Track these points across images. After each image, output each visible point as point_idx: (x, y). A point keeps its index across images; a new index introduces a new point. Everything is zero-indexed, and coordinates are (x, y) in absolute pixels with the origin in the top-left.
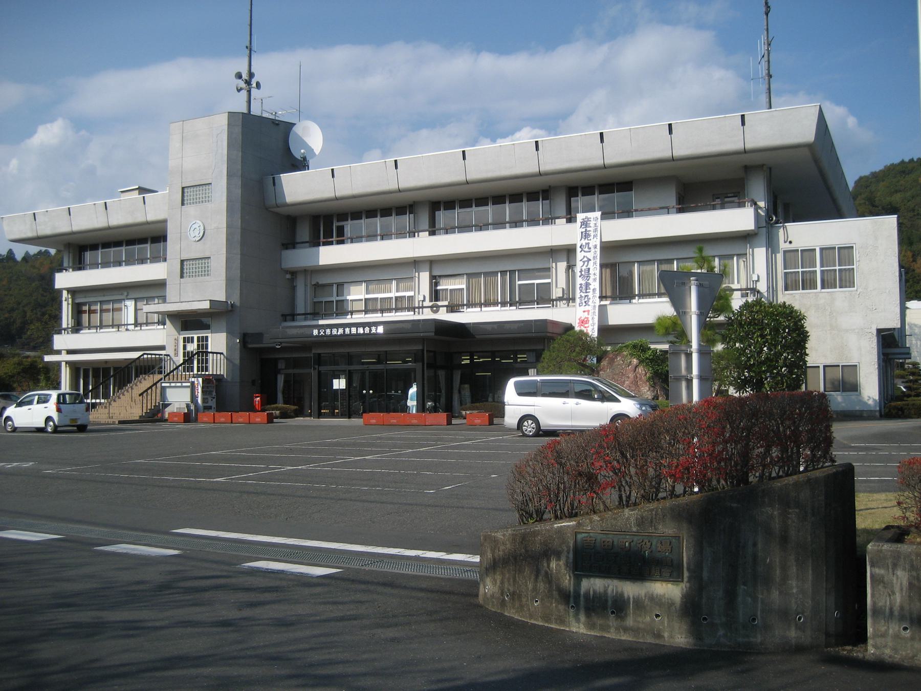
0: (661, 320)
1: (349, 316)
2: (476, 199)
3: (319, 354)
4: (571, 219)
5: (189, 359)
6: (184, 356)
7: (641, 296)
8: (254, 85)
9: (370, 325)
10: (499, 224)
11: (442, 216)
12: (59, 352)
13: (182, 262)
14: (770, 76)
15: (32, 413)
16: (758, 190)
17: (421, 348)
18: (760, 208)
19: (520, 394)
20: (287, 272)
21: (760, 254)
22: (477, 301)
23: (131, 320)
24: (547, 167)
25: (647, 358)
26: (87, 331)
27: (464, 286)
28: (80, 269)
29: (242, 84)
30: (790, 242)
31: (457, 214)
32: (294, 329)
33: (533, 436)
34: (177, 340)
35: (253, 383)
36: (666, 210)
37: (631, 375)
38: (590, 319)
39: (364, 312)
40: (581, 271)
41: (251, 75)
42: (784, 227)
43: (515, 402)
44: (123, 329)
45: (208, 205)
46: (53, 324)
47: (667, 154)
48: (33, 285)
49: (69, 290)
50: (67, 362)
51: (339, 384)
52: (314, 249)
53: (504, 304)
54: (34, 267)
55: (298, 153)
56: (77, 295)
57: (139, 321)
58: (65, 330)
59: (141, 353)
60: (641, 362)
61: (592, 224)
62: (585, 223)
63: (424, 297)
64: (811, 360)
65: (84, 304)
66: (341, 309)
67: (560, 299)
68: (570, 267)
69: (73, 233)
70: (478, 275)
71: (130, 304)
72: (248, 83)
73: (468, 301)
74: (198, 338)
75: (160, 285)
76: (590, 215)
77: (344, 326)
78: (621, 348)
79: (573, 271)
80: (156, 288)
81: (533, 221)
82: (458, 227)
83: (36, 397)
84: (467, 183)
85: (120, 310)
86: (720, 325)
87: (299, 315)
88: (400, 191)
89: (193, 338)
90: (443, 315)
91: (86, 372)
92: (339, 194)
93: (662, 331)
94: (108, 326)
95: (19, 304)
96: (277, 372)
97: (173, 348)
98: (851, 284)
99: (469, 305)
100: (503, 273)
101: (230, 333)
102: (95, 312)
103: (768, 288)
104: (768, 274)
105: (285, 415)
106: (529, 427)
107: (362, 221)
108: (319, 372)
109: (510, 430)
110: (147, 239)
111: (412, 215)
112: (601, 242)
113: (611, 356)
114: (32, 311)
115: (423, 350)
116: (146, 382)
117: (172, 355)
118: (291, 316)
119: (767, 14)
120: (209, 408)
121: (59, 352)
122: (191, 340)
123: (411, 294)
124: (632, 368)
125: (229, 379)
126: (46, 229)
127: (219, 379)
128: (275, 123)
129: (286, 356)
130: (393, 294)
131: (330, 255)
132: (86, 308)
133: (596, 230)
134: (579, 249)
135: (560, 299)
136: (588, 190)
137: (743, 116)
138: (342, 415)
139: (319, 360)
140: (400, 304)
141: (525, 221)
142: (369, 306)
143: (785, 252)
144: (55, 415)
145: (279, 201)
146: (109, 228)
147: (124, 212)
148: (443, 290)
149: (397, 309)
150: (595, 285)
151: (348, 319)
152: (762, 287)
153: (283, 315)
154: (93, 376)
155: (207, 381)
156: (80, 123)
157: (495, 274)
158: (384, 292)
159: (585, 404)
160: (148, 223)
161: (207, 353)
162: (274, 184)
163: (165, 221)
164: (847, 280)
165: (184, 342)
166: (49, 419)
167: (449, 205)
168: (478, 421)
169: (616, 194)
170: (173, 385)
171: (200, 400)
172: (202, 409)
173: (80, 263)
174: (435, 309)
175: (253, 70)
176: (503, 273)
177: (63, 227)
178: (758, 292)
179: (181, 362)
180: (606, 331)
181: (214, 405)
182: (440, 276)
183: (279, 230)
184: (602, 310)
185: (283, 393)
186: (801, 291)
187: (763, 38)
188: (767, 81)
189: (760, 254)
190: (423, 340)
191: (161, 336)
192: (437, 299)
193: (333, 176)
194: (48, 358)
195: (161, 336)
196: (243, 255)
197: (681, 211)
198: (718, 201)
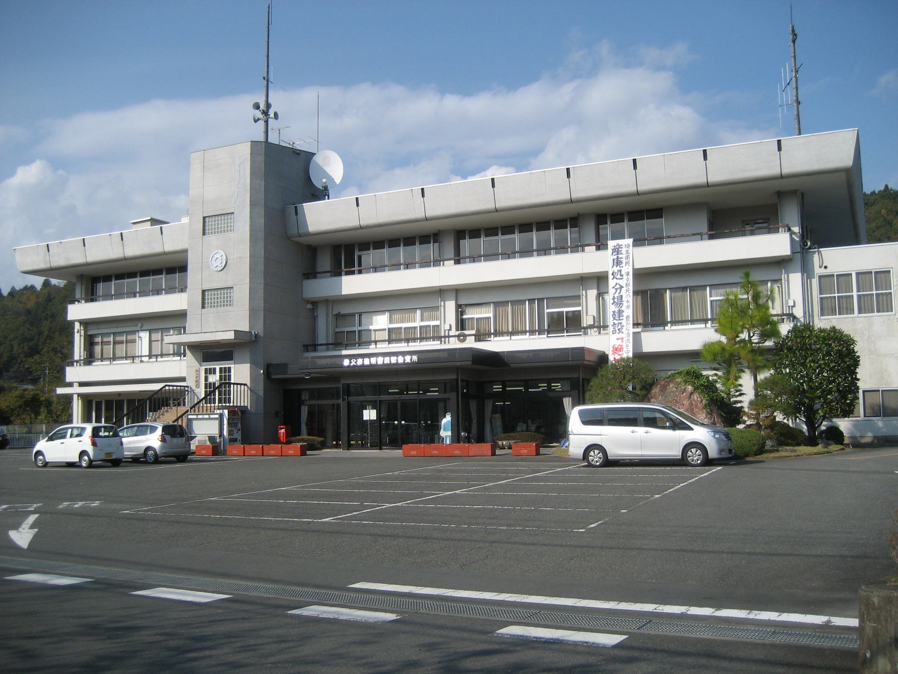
0: (708, 346)
1: (373, 346)
2: (405, 239)
3: (348, 385)
4: (601, 245)
5: (211, 389)
6: (206, 388)
7: (674, 323)
8: (272, 115)
9: (396, 354)
10: (526, 252)
11: (466, 244)
12: (70, 385)
13: (204, 292)
14: (798, 103)
15: (66, 447)
16: (791, 214)
17: (455, 377)
18: (795, 233)
19: (585, 423)
20: (308, 301)
21: (795, 279)
22: (505, 330)
23: (146, 352)
24: (502, 204)
25: (701, 385)
26: (99, 363)
27: (491, 315)
28: (92, 300)
29: (259, 114)
30: (826, 267)
31: (482, 242)
32: (322, 357)
33: (600, 466)
34: (198, 371)
35: (277, 414)
36: (699, 236)
37: (686, 403)
38: (624, 346)
39: (385, 345)
40: (614, 298)
41: (268, 106)
42: (819, 252)
43: (580, 434)
44: (137, 360)
45: (230, 234)
46: (68, 359)
47: (702, 180)
48: (20, 319)
49: (82, 322)
50: (79, 395)
51: (370, 414)
52: (336, 278)
53: (532, 332)
54: (21, 302)
55: (318, 183)
56: (90, 327)
57: (153, 353)
58: (77, 362)
59: (162, 385)
60: (696, 389)
61: (624, 250)
62: (617, 250)
63: (450, 326)
64: (863, 385)
65: (96, 335)
66: (360, 339)
67: (591, 327)
68: (600, 295)
69: (87, 264)
70: (505, 303)
71: (145, 335)
72: (266, 113)
73: (495, 330)
74: (221, 369)
75: (181, 315)
76: (620, 242)
77: (369, 356)
78: (673, 375)
79: (603, 299)
80: (175, 319)
81: (561, 249)
82: (537, 251)
83: (70, 431)
84: (497, 210)
85: (134, 341)
86: (769, 350)
87: (321, 345)
88: (426, 219)
89: (215, 369)
90: (470, 343)
91: (99, 404)
92: (364, 223)
93: (710, 358)
94: (121, 358)
95: (6, 338)
96: (301, 403)
97: (195, 379)
98: (889, 308)
99: (497, 333)
100: (531, 301)
101: (254, 364)
102: (108, 343)
103: (805, 313)
104: (804, 299)
105: (312, 447)
106: (596, 457)
107: (385, 250)
108: (348, 402)
109: (576, 460)
110: (169, 269)
111: (436, 245)
112: (633, 269)
113: (663, 383)
114: (19, 345)
115: (457, 380)
116: (169, 416)
117: (194, 388)
118: (313, 346)
119: (794, 42)
120: (235, 440)
121: (70, 385)
122: (213, 371)
123: (437, 323)
124: (687, 397)
125: (253, 411)
126: (60, 259)
127: (243, 410)
128: (297, 153)
129: (311, 387)
130: (417, 324)
131: (352, 284)
132: (98, 340)
133: (627, 257)
134: (611, 277)
135: (591, 327)
136: (617, 217)
137: (705, 151)
138: (373, 446)
139: (348, 391)
140: (425, 334)
141: (553, 249)
142: (393, 336)
143: (820, 277)
144: (90, 449)
145: (301, 231)
146: (125, 259)
147: (140, 243)
148: (469, 319)
149: (422, 339)
150: (628, 312)
151: (372, 349)
152: (799, 312)
153: (304, 346)
154: (106, 410)
155: (233, 412)
156: (57, 163)
157: (523, 302)
158: (408, 321)
159: (654, 432)
160: (165, 253)
161: (230, 384)
162: (297, 214)
163: (185, 252)
164: (884, 304)
165: (206, 373)
166: (83, 453)
167: (475, 233)
168: (524, 451)
169: (646, 221)
170: (200, 417)
171: (225, 433)
172: (227, 441)
173: (92, 294)
174: (462, 338)
175: (270, 101)
176: (531, 301)
177: (76, 257)
178: (794, 317)
179: (203, 396)
180: (640, 356)
181: (239, 438)
182: (467, 305)
183: (302, 260)
184: (637, 337)
185: (307, 424)
186: (838, 316)
187: (788, 66)
188: (795, 108)
189: (795, 279)
190: (457, 369)
191: (184, 369)
192: (463, 329)
193: (358, 205)
194: (60, 391)
195: (184, 369)
196: (266, 285)
197: (712, 237)
198: (748, 228)
